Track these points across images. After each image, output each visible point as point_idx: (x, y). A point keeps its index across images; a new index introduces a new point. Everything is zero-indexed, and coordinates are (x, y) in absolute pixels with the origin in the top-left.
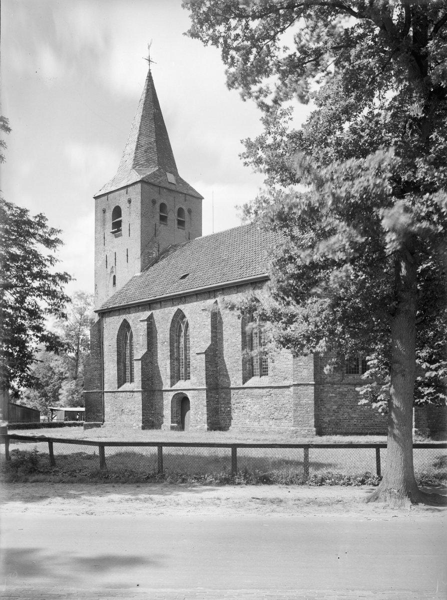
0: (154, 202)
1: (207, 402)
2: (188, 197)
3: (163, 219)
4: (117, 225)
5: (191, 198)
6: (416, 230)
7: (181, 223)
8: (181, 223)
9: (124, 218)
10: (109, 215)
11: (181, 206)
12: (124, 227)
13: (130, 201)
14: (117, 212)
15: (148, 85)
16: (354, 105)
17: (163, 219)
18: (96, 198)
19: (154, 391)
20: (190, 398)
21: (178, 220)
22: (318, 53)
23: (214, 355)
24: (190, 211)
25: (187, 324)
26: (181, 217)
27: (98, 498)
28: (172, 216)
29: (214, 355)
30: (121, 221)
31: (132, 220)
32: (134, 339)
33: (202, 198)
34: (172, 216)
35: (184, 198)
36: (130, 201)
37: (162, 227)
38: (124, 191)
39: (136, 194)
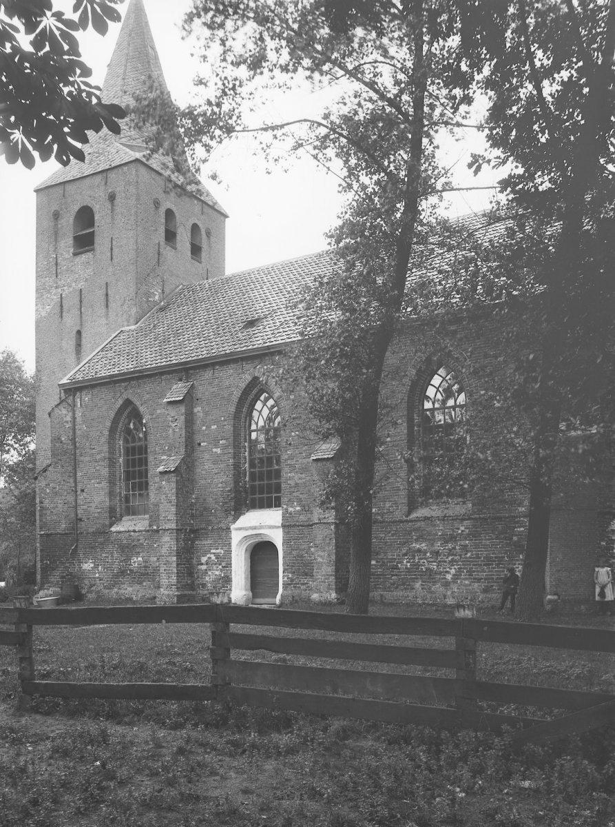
0: (157, 204)
2: (206, 209)
3: (170, 236)
4: (84, 242)
5: (210, 211)
7: (196, 250)
8: (196, 250)
10: (68, 221)
11: (196, 222)
13: (112, 198)
14: (86, 216)
16: (9, 476)
17: (170, 236)
23: (185, 475)
24: (208, 234)
27: (243, 558)
28: (184, 237)
29: (185, 475)
30: (92, 234)
33: (226, 216)
34: (184, 237)
35: (200, 208)
36: (112, 198)
37: (168, 252)
38: (98, 179)
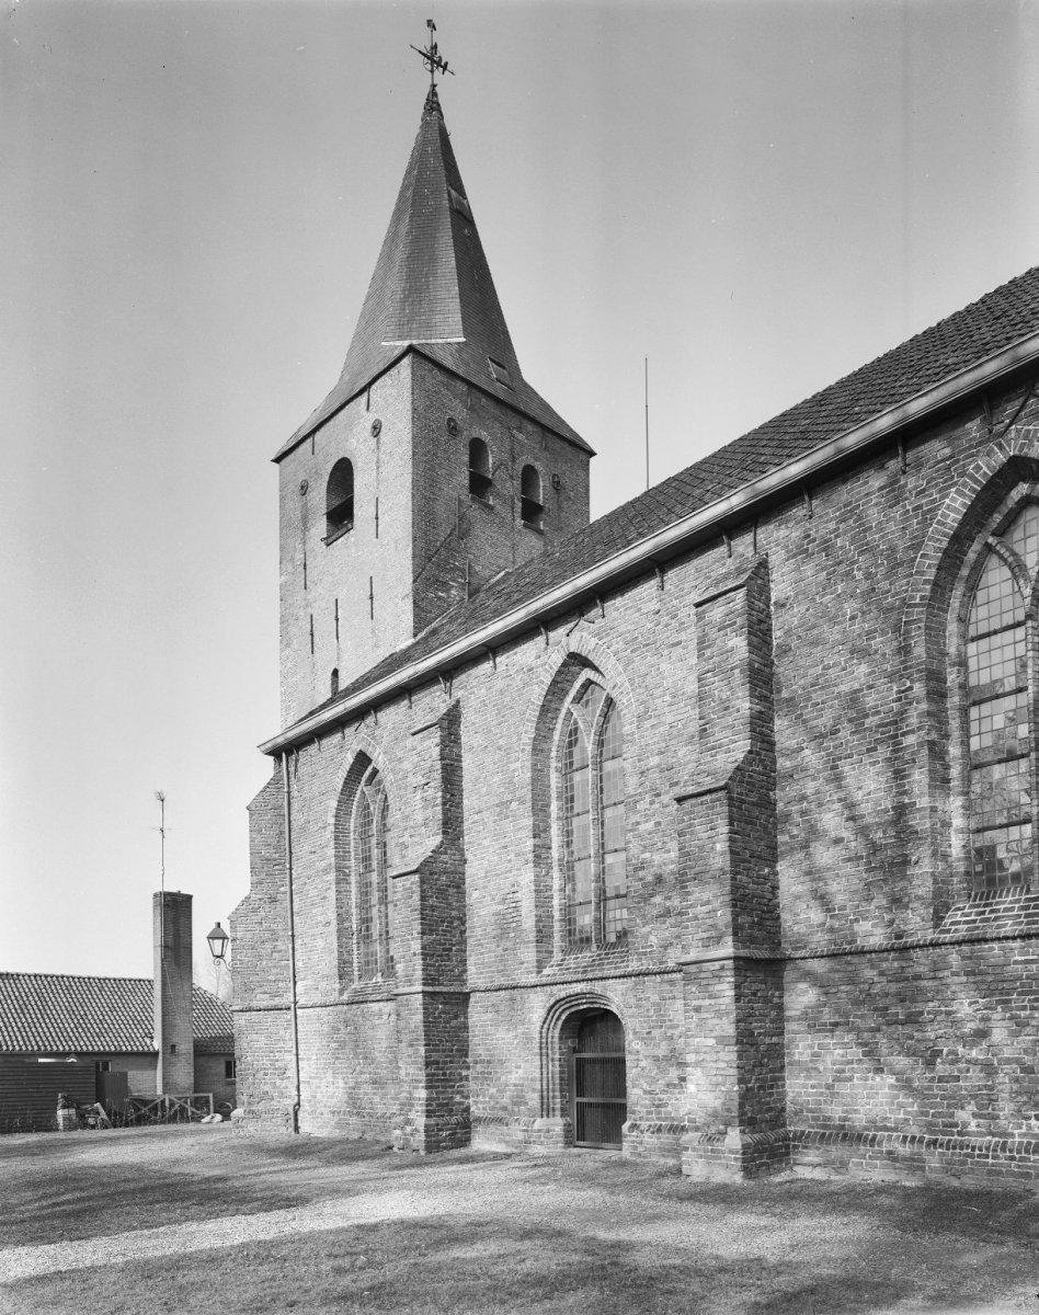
4: (341, 515)
10: (319, 498)
11: (531, 461)
13: (376, 429)
14: (343, 474)
18: (278, 460)
36: (376, 429)
39: (395, 398)
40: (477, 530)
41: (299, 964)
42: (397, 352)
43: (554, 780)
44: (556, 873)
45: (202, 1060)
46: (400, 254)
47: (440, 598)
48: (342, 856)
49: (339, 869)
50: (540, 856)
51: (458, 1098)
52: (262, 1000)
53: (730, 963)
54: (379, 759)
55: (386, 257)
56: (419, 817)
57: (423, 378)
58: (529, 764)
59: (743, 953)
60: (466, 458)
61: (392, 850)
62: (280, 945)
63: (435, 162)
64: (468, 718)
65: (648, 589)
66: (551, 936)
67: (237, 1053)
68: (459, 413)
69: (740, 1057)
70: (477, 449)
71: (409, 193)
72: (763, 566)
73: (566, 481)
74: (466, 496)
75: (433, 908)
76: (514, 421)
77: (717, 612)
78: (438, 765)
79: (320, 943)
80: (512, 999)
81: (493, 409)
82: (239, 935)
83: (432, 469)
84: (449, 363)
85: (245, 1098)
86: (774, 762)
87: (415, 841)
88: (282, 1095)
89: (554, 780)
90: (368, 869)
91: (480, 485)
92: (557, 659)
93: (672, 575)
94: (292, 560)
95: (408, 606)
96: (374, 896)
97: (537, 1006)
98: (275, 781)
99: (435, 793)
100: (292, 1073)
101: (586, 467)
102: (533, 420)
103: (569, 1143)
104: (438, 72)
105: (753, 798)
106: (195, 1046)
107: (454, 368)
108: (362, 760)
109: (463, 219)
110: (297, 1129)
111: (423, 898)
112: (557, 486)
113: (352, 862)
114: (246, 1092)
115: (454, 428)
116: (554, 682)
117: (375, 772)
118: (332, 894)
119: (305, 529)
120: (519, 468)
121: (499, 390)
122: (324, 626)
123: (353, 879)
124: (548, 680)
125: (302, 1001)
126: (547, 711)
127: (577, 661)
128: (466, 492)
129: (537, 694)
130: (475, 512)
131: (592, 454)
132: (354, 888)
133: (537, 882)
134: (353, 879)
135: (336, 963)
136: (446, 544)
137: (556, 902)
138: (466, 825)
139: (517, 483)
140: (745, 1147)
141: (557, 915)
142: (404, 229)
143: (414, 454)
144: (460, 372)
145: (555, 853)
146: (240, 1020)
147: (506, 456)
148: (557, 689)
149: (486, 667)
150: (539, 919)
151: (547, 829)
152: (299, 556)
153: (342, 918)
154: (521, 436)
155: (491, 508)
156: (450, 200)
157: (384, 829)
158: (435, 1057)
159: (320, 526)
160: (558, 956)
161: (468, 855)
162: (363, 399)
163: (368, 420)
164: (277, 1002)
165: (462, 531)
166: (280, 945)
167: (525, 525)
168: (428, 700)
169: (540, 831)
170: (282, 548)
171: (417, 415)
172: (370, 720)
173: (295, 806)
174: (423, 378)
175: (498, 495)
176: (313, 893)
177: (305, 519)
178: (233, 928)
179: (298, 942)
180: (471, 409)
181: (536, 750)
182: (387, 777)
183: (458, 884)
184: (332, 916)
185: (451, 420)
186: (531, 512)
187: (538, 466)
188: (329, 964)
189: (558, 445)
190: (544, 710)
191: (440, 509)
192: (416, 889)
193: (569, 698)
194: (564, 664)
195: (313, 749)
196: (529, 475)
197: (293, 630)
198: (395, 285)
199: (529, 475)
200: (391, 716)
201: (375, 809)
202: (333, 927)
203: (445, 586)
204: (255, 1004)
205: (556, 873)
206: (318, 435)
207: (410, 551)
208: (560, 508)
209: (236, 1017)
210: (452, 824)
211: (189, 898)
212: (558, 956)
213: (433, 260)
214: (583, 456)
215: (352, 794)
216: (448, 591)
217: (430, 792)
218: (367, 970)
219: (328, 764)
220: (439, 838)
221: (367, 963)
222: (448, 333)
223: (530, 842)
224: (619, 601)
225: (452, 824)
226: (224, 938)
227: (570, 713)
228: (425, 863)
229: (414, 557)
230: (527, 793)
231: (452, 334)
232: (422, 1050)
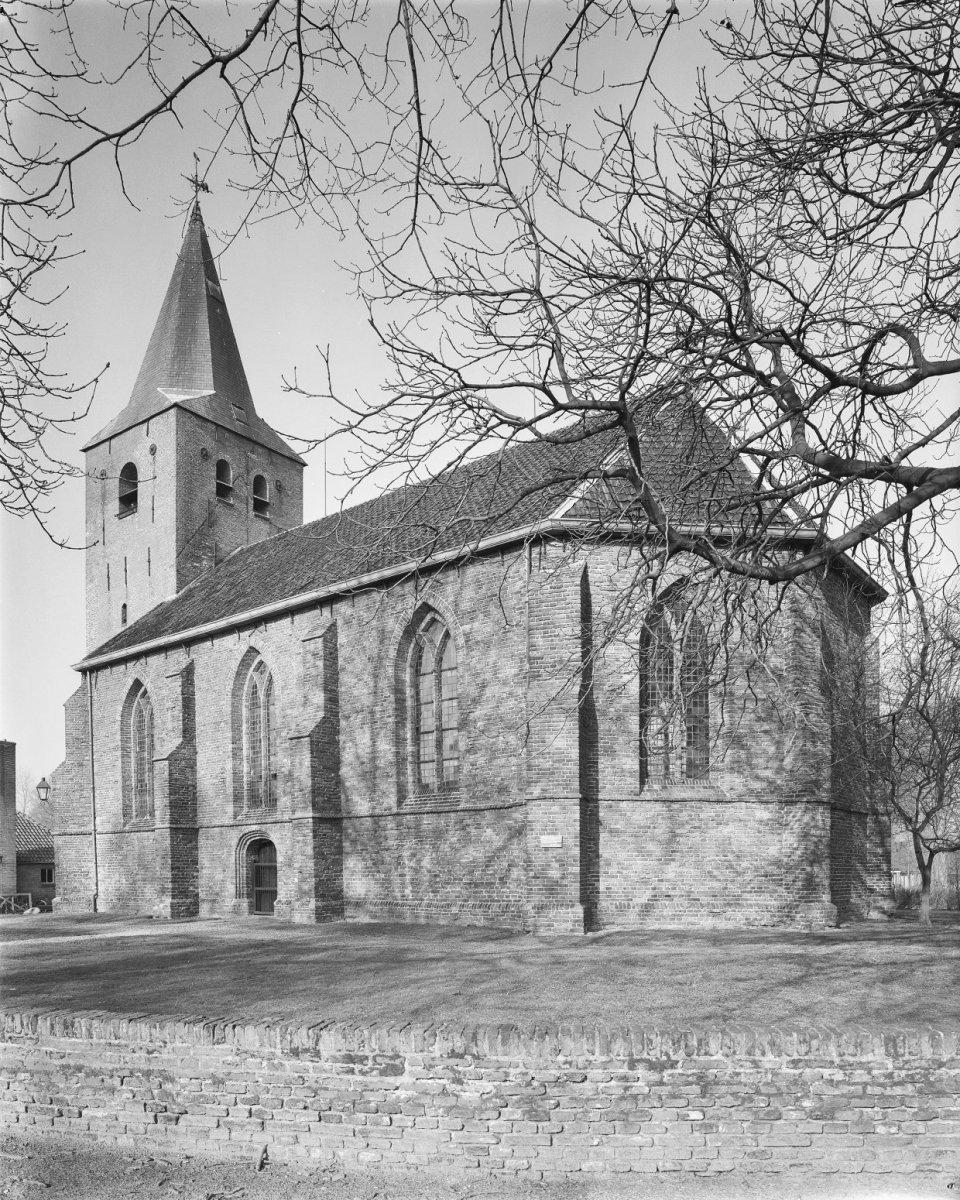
1: (315, 848)
4: (129, 501)
6: (857, 842)
9: (144, 491)
10: (114, 486)
11: (261, 473)
12: (143, 501)
13: (153, 450)
14: (130, 472)
15: (191, 231)
18: (85, 450)
19: (197, 831)
20: (275, 842)
21: (255, 499)
22: (810, 926)
25: (270, 681)
26: (261, 495)
30: (136, 492)
31: (160, 492)
32: (157, 721)
36: (153, 450)
39: (165, 433)
40: (222, 520)
41: (97, 806)
42: (167, 404)
43: (245, 712)
44: (245, 763)
45: (23, 868)
46: (173, 324)
47: (195, 567)
48: (125, 740)
49: (123, 749)
50: (236, 754)
51: (191, 888)
52: (74, 829)
53: (311, 820)
54: (148, 684)
55: (166, 310)
56: (170, 726)
57: (184, 423)
58: (230, 703)
59: (317, 815)
60: (214, 474)
61: (157, 743)
62: (85, 793)
63: (197, 258)
64: (198, 671)
65: (286, 622)
66: (242, 798)
67: (56, 861)
68: (209, 443)
69: (316, 865)
70: (222, 468)
71: (179, 279)
72: (333, 626)
73: (286, 484)
74: (214, 498)
75: (176, 780)
76: (249, 446)
77: (311, 646)
78: (180, 698)
79: (111, 794)
80: (221, 833)
81: (234, 440)
82: (58, 787)
83: (190, 482)
84: (202, 412)
85: (61, 890)
86: (338, 721)
87: (168, 741)
88: (86, 889)
89: (245, 712)
90: (142, 749)
91: (223, 491)
92: (244, 648)
93: (297, 617)
94: (95, 522)
95: (173, 572)
96: (145, 765)
97: (234, 837)
98: (82, 688)
99: (178, 712)
100: (92, 875)
101: (301, 471)
102: (263, 446)
103: (251, 913)
104: (202, 194)
105: (326, 740)
106: (18, 857)
107: (205, 416)
108: (137, 684)
109: (217, 302)
110: (96, 910)
111: (170, 775)
112: (279, 488)
113: (132, 745)
114: (62, 886)
115: (206, 455)
116: (243, 660)
117: (145, 692)
118: (119, 764)
119: (104, 504)
120: (252, 478)
121: (238, 427)
122: (117, 572)
123: (133, 755)
124: (240, 659)
125: (99, 829)
126: (240, 675)
127: (253, 651)
128: (214, 495)
129: (234, 665)
130: (219, 509)
131: (305, 465)
132: (133, 760)
133: (234, 768)
134: (133, 755)
135: (121, 806)
136: (200, 532)
137: (245, 779)
138: (198, 732)
139: (251, 487)
140: (317, 908)
141: (245, 787)
142: (175, 306)
143: (178, 473)
144: (210, 418)
145: (245, 752)
146: (58, 841)
147: (242, 470)
148: (245, 663)
149: (209, 643)
150: (235, 789)
151: (240, 739)
152: (100, 521)
153: (125, 778)
154: (254, 456)
155: (232, 506)
156: (207, 289)
157: (152, 726)
158: (177, 864)
159: (114, 506)
160: (246, 810)
161: (198, 750)
162: (145, 426)
163: (148, 443)
164: (83, 829)
165: (211, 522)
166: (85, 793)
167: (256, 516)
168: (176, 655)
169: (236, 740)
170: (87, 513)
171: (180, 449)
172: (143, 661)
173: (95, 707)
174: (184, 423)
175: (237, 497)
176: (107, 762)
177: (104, 496)
178: (54, 782)
179: (97, 792)
180: (218, 441)
181: (234, 695)
182: (153, 698)
183: (192, 766)
184: (119, 778)
185: (203, 449)
186: (260, 506)
187: (265, 475)
188: (116, 806)
189: (280, 460)
190: (238, 674)
191: (196, 509)
192: (167, 769)
193: (252, 669)
194: (248, 651)
195: (107, 671)
196: (259, 483)
197: (95, 572)
198: (169, 349)
199: (259, 483)
200: (155, 661)
201: (146, 714)
202: (120, 784)
203: (198, 559)
204: (68, 830)
205: (245, 763)
206: (113, 441)
207: (174, 536)
208: (282, 503)
209: (56, 838)
210: (188, 732)
211: (14, 745)
212: (246, 810)
213: (194, 331)
214: (298, 467)
215: (131, 707)
216: (200, 562)
217: (176, 713)
218: (141, 812)
219: (116, 682)
220: (181, 740)
221: (141, 807)
222: (202, 389)
223: (231, 746)
224: (273, 625)
225: (188, 732)
226: (48, 788)
227: (252, 678)
228: (171, 755)
229: (177, 540)
230: (228, 718)
231: (206, 387)
232: (170, 861)
